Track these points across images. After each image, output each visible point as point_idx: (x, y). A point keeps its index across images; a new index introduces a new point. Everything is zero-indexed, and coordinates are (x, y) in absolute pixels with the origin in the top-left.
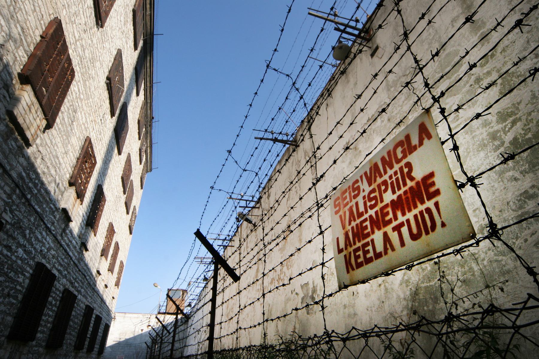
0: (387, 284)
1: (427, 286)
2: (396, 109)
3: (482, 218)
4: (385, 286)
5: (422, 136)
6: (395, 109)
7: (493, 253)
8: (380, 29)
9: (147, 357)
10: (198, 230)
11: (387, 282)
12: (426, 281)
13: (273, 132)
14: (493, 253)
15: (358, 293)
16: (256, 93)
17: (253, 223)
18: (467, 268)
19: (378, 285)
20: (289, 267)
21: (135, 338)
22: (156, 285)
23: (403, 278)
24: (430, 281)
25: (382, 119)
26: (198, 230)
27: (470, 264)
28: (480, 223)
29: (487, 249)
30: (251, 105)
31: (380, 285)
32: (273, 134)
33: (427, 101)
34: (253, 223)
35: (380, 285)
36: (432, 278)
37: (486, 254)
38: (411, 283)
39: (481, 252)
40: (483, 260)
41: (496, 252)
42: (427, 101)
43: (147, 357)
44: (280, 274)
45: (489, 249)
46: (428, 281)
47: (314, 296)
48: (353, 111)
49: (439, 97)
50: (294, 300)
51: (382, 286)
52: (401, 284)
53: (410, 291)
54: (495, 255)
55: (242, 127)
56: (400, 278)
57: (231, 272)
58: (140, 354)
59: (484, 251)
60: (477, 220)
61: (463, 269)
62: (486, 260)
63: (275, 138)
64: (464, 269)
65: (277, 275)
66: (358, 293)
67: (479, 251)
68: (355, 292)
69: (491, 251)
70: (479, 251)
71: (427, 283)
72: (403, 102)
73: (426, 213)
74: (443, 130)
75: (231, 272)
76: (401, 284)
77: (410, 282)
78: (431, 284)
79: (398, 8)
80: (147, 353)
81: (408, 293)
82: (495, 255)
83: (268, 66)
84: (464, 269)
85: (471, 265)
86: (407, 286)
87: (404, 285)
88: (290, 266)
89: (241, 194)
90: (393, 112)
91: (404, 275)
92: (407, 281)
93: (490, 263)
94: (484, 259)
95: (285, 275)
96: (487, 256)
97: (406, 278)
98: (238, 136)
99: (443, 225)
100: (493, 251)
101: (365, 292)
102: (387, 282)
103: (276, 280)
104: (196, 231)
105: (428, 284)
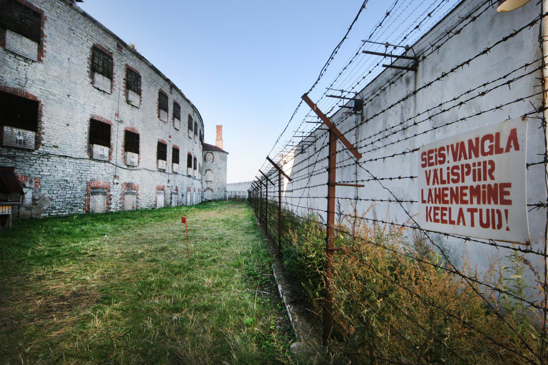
99: (508, 229)
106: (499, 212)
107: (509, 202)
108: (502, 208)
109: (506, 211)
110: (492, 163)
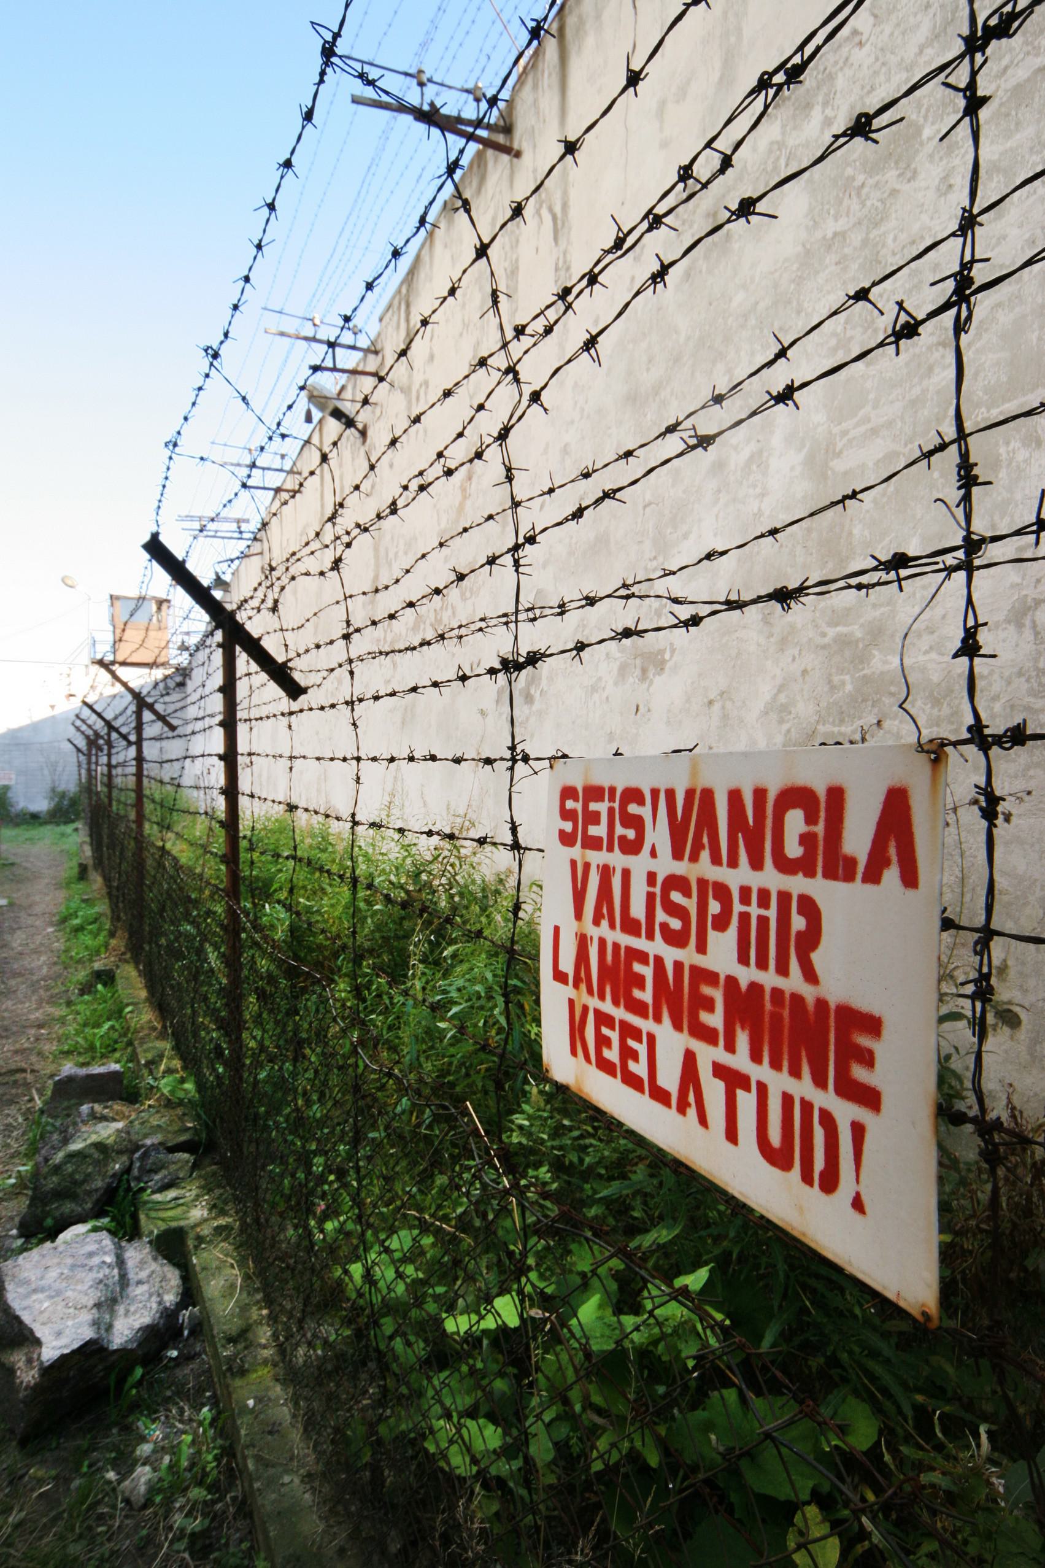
0: (729, 704)
1: (833, 732)
2: (888, 80)
3: (1034, 580)
4: (723, 707)
5: (885, 848)
6: (882, 78)
7: (1026, 686)
8: (858, 140)
9: (80, 775)
10: (155, 537)
11: (730, 699)
12: (831, 720)
13: (424, 78)
14: (1026, 686)
15: (649, 710)
16: (288, 164)
17: (360, 426)
18: (946, 710)
19: (706, 700)
20: (468, 594)
21: (35, 727)
22: (70, 583)
23: (775, 698)
24: (842, 721)
25: (829, 112)
26: (155, 537)
27: (957, 702)
28: (1024, 592)
29: (1015, 670)
30: (271, 207)
31: (711, 702)
32: (421, 84)
33: (1006, 69)
34: (360, 426)
35: (711, 702)
36: (849, 716)
37: (1009, 683)
38: (792, 716)
39: (996, 676)
40: (996, 698)
41: (1035, 685)
42: (1006, 69)
43: (80, 775)
44: (442, 608)
45: (1020, 674)
46: (837, 722)
47: (532, 691)
48: (733, 39)
49: (998, 740)
50: (476, 690)
51: (717, 707)
52: (767, 713)
53: (786, 735)
54: (1032, 693)
55: (247, 279)
56: (768, 697)
57: (280, 674)
58: (60, 769)
59: (1007, 674)
60: (1019, 581)
61: (935, 711)
62: (1003, 701)
63: (432, 104)
64: (940, 710)
65: (432, 611)
66: (649, 710)
67: (992, 673)
68: (641, 707)
69: (1023, 679)
70: (992, 673)
71: (833, 724)
72: (921, 52)
73: (821, 1123)
74: (1021, 226)
75: (280, 674)
76: (767, 713)
77: (790, 713)
78: (843, 729)
79: (974, 74)
80: (79, 766)
81: (779, 739)
82: (1032, 693)
83: (328, 52)
84: (940, 710)
85: (960, 704)
86: (781, 721)
87: (774, 716)
88: (471, 590)
89: (312, 320)
90: (872, 89)
91: (779, 691)
92: (784, 709)
93: (1008, 710)
94: (998, 696)
95: (454, 613)
96: (1009, 689)
97: (782, 698)
98: (236, 307)
100: (1028, 681)
101: (669, 711)
102: (730, 699)
103: (428, 622)
104: (147, 538)
105: (836, 729)
106: (828, 1120)
107: (870, 1098)
108: (845, 1112)
109: (858, 1131)
110: (809, 907)
